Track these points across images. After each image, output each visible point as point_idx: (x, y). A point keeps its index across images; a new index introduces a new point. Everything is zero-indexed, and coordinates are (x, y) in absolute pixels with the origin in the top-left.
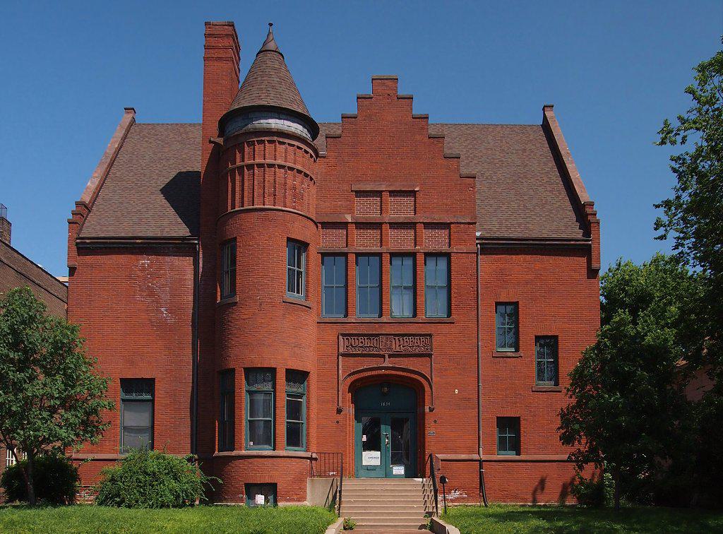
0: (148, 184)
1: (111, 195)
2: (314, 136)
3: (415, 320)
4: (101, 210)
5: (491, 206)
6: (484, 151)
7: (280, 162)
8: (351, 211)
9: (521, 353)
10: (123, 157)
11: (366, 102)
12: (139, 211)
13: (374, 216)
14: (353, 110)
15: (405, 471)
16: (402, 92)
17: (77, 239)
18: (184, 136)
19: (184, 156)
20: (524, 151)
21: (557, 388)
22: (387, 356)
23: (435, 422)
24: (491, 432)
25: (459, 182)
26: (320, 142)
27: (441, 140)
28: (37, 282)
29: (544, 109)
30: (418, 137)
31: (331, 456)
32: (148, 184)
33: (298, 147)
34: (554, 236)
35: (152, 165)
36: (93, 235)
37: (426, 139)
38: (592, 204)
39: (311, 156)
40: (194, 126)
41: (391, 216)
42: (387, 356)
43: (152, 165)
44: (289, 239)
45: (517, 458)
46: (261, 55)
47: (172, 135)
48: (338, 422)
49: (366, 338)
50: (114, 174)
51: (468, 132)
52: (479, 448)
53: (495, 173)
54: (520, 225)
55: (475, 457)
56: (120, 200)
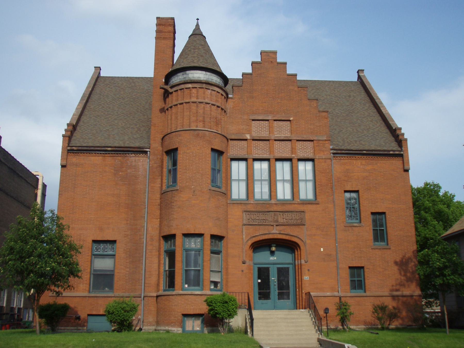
0: (112, 113)
1: (88, 119)
2: (225, 85)
3: (294, 202)
4: (82, 129)
5: (335, 129)
6: (325, 97)
7: (194, 100)
8: (249, 132)
9: (363, 224)
10: (94, 97)
11: (257, 66)
12: (108, 130)
13: (265, 134)
14: (249, 70)
15: (188, 286)
16: (279, 60)
17: (68, 147)
18: (133, 84)
19: (134, 97)
20: (350, 96)
21: (388, 247)
22: (275, 226)
23: (309, 270)
24: (345, 274)
25: (318, 115)
26: (229, 88)
27: (306, 89)
28: (20, 174)
29: (358, 72)
30: (291, 88)
31: (240, 294)
32: (112, 113)
33: (217, 92)
34: (379, 148)
35: (114, 101)
36: (79, 145)
37: (296, 89)
38: (400, 129)
39: (225, 98)
40: (139, 79)
41: (277, 135)
42: (275, 226)
43: (114, 101)
44: (213, 150)
45: (364, 294)
46: (192, 37)
47: (125, 84)
48: (242, 271)
49: (261, 214)
50: (89, 107)
51: (313, 85)
52: (338, 288)
53: (334, 110)
54: (356, 141)
55: (336, 294)
56: (95, 123)
